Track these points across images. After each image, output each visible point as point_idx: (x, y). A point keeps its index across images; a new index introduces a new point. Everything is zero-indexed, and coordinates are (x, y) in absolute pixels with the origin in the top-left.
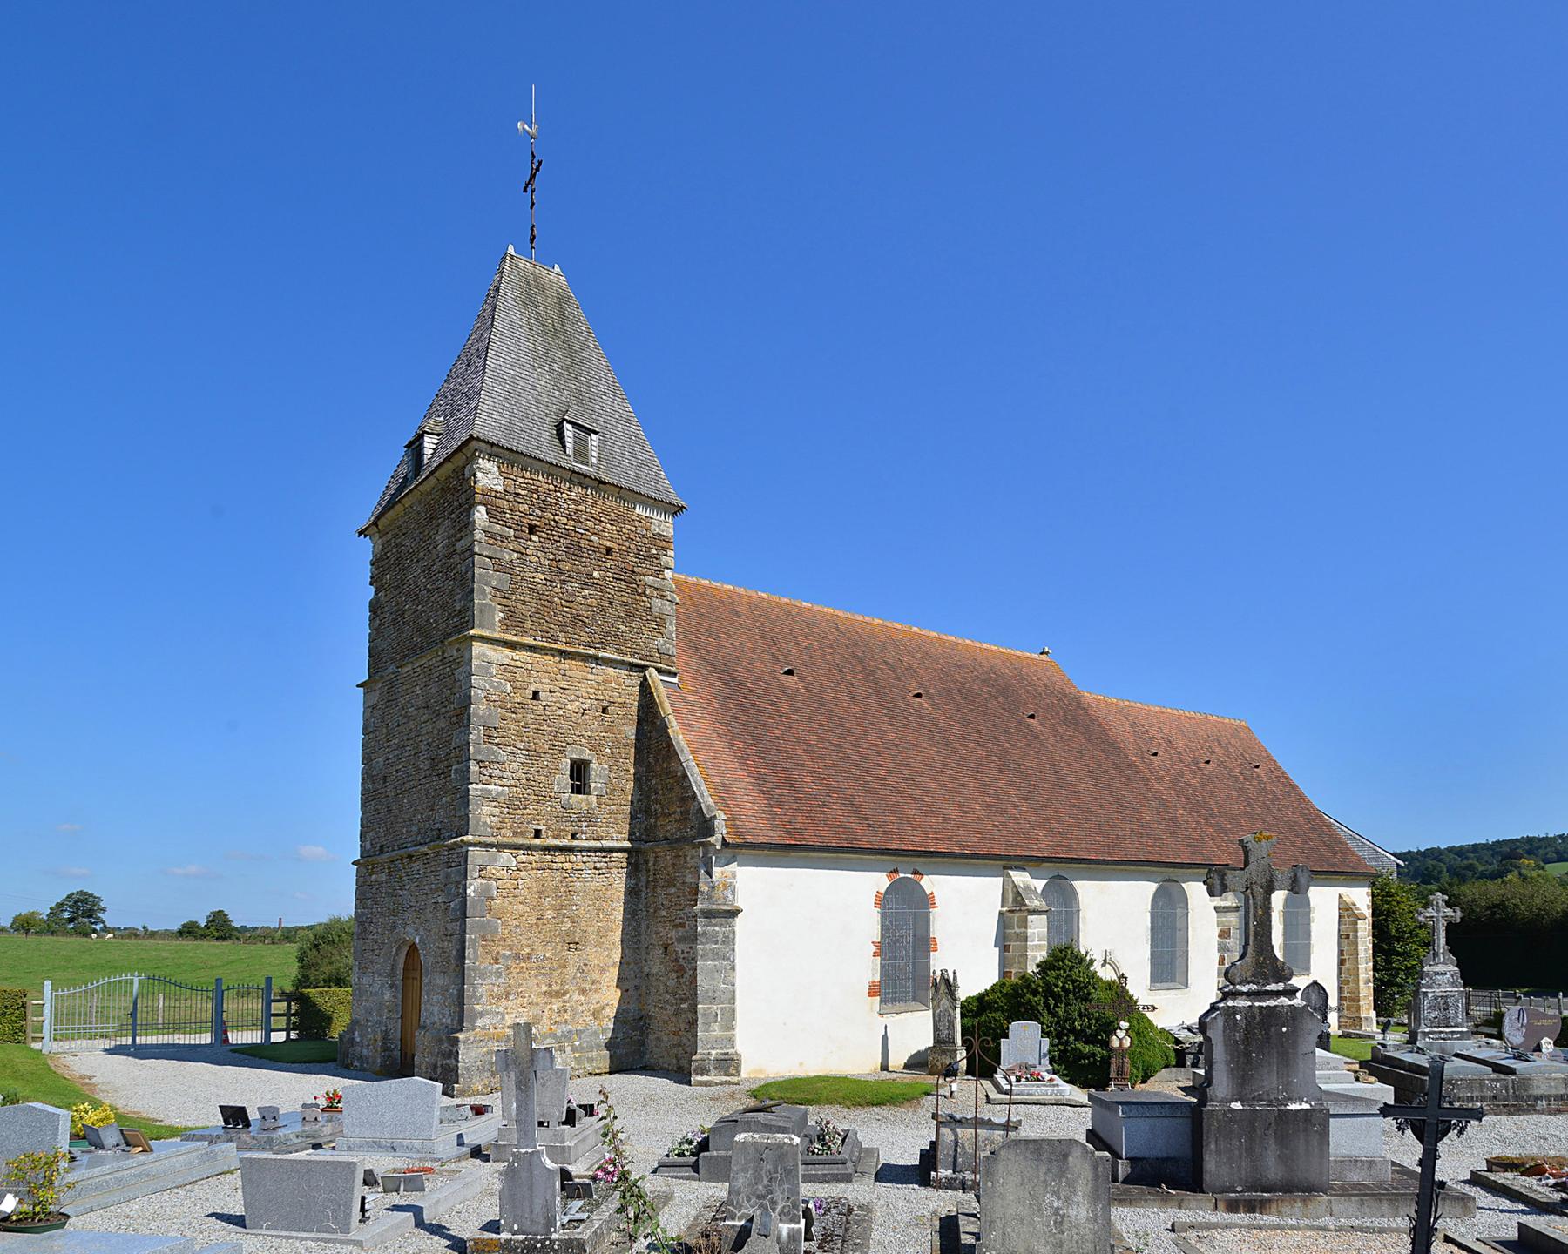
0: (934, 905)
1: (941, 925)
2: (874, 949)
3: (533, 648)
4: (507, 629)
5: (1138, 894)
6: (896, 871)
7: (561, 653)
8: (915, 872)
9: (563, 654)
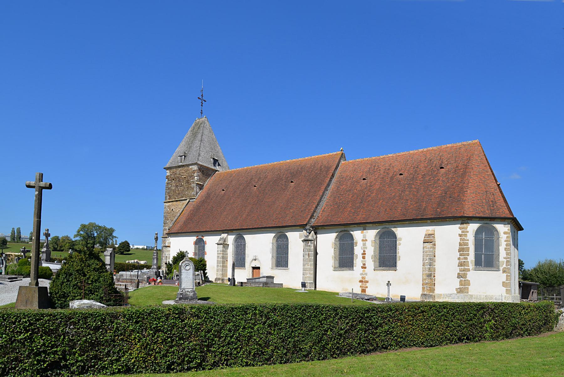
0: (206, 244)
1: (207, 248)
2: (193, 254)
3: (172, 201)
4: (169, 199)
5: (372, 234)
6: (198, 236)
7: (177, 201)
8: (202, 236)
9: (177, 201)
